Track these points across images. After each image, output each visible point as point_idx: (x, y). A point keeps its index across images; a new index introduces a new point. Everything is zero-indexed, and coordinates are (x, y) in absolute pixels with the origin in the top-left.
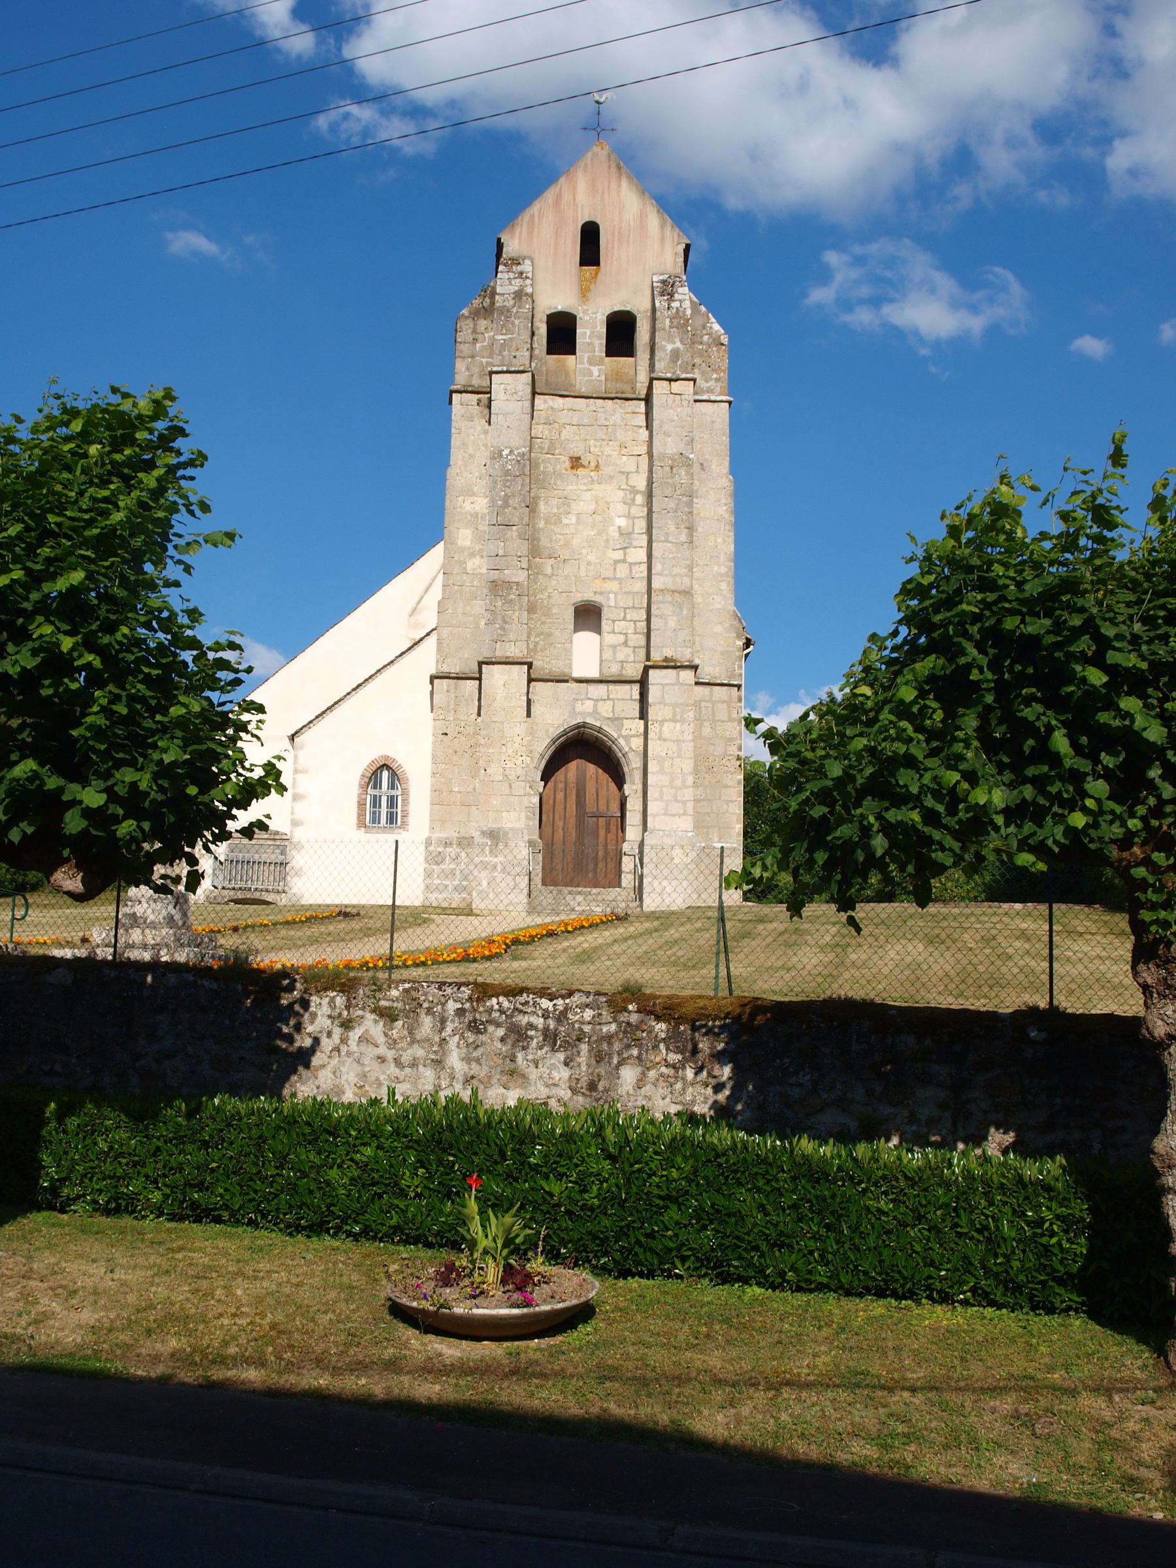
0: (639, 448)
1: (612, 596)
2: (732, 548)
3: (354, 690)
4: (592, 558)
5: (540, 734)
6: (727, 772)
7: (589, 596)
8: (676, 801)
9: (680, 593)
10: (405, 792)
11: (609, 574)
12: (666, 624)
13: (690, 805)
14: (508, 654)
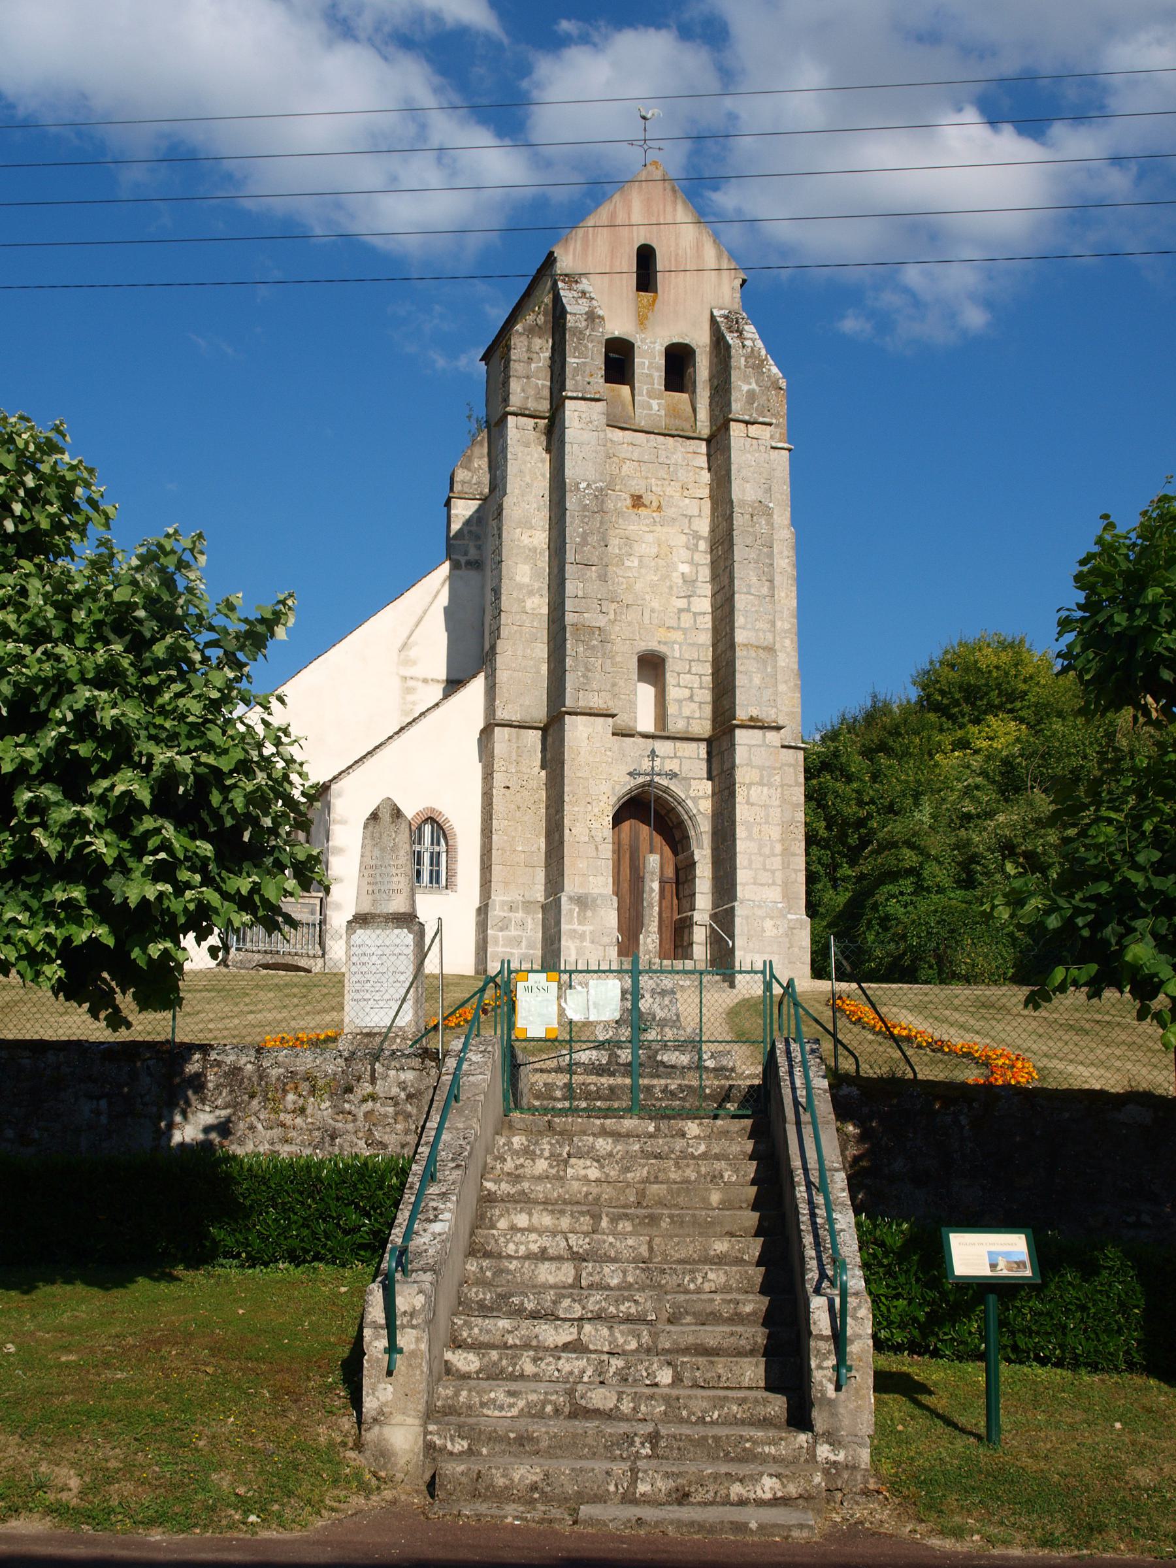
0: (701, 491)
1: (676, 647)
2: (794, 603)
3: (397, 733)
4: (655, 604)
6: (795, 839)
7: (653, 645)
8: (765, 870)
9: (764, 649)
11: (672, 623)
12: (751, 681)
13: (778, 875)
14: (592, 704)
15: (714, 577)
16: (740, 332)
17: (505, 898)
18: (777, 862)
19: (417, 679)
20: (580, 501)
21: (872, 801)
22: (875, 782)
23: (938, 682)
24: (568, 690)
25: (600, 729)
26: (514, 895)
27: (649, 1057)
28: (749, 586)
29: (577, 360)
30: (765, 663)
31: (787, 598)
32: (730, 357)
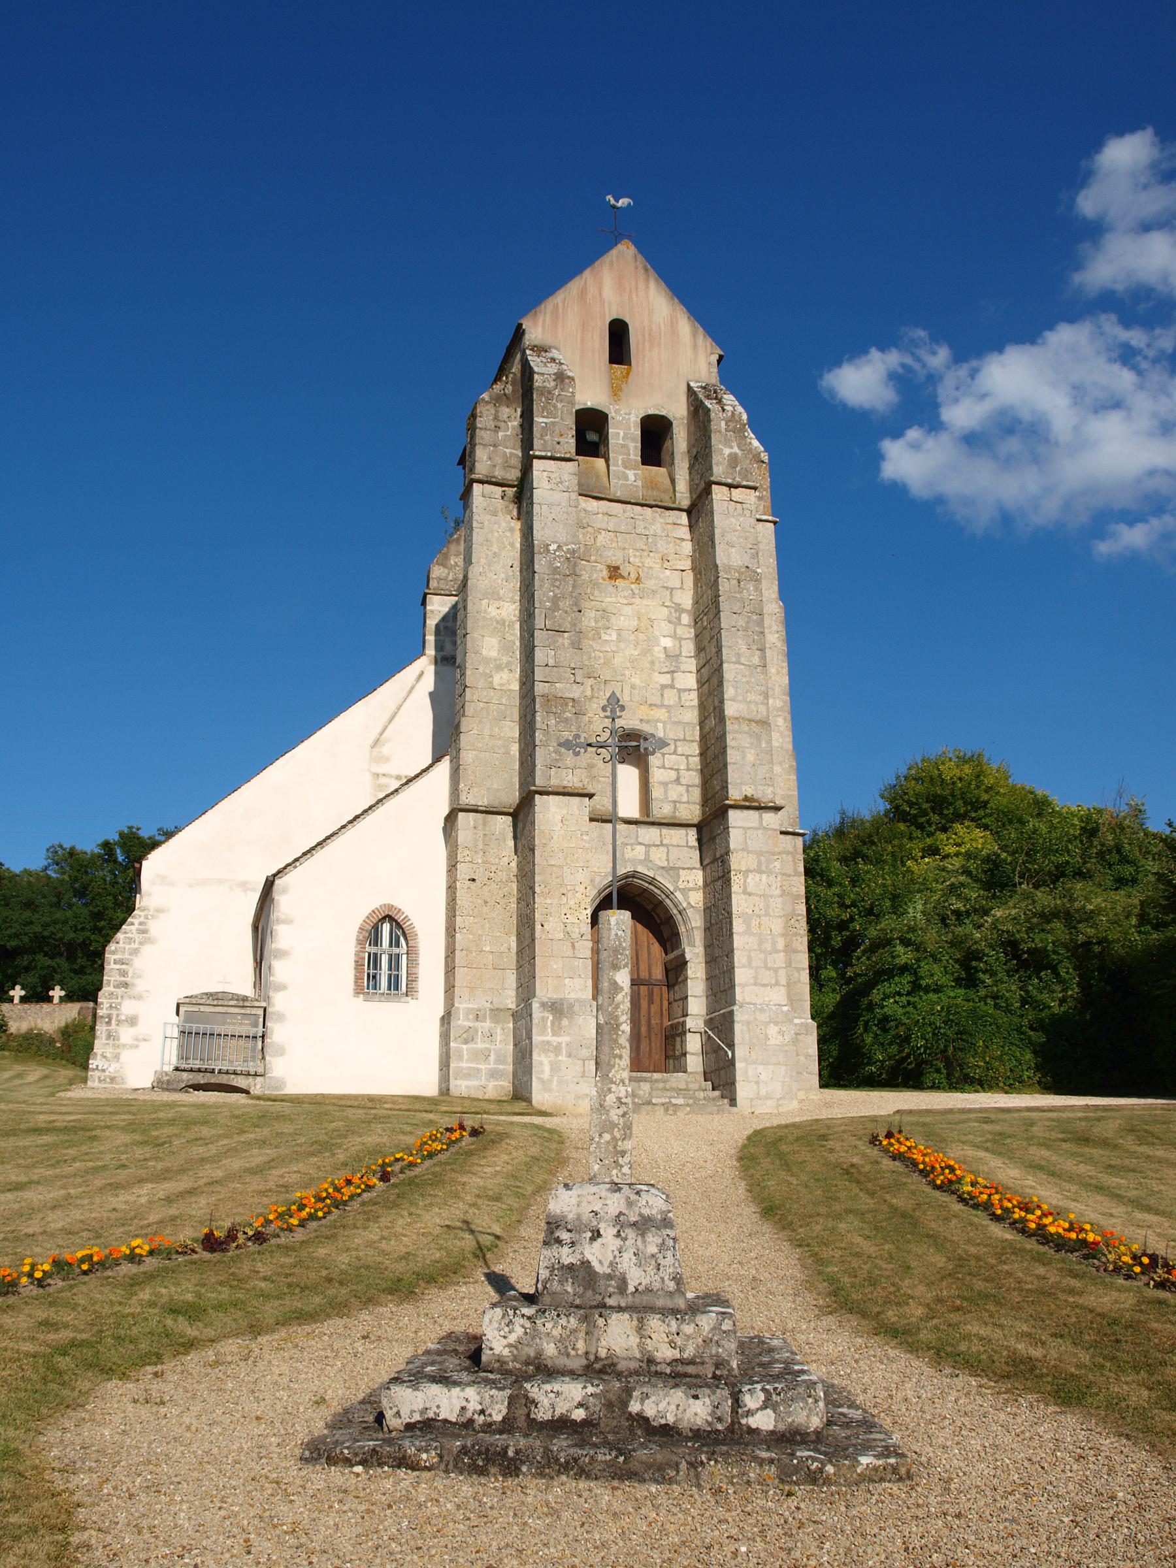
0: (683, 562)
1: (660, 725)
2: (786, 680)
3: (351, 822)
4: (636, 680)
6: (796, 934)
8: (767, 968)
9: (756, 722)
10: (412, 952)
11: (656, 700)
12: (744, 758)
13: (782, 973)
14: (565, 783)
15: (700, 649)
16: (720, 401)
17: (471, 1006)
18: (779, 960)
19: (391, 776)
20: (551, 563)
21: (854, 904)
22: (854, 886)
23: (906, 794)
24: (538, 767)
25: (575, 810)
26: (482, 1002)
27: (609, 1405)
28: (739, 655)
29: (545, 420)
30: (758, 738)
31: (779, 675)
32: (709, 421)
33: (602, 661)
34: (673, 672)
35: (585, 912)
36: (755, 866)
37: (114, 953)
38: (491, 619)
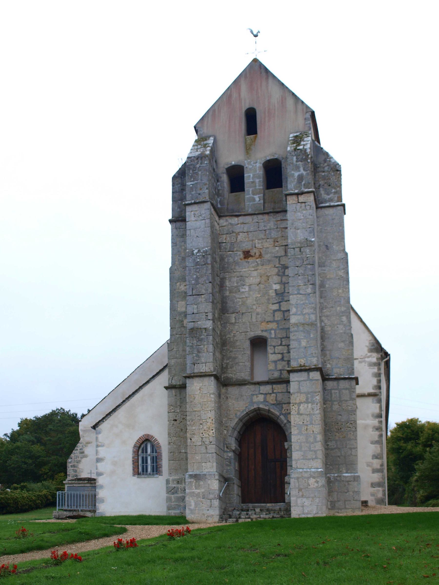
1: (273, 332)
4: (259, 310)
5: (231, 416)
7: (259, 333)
14: (202, 371)
17: (176, 477)
29: (192, 183)
33: (240, 303)
34: (280, 302)
35: (212, 431)
36: (304, 400)
37: (70, 463)
38: (182, 292)
